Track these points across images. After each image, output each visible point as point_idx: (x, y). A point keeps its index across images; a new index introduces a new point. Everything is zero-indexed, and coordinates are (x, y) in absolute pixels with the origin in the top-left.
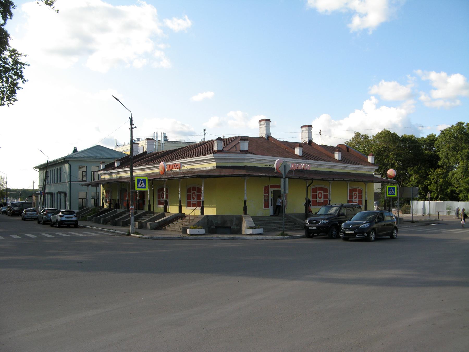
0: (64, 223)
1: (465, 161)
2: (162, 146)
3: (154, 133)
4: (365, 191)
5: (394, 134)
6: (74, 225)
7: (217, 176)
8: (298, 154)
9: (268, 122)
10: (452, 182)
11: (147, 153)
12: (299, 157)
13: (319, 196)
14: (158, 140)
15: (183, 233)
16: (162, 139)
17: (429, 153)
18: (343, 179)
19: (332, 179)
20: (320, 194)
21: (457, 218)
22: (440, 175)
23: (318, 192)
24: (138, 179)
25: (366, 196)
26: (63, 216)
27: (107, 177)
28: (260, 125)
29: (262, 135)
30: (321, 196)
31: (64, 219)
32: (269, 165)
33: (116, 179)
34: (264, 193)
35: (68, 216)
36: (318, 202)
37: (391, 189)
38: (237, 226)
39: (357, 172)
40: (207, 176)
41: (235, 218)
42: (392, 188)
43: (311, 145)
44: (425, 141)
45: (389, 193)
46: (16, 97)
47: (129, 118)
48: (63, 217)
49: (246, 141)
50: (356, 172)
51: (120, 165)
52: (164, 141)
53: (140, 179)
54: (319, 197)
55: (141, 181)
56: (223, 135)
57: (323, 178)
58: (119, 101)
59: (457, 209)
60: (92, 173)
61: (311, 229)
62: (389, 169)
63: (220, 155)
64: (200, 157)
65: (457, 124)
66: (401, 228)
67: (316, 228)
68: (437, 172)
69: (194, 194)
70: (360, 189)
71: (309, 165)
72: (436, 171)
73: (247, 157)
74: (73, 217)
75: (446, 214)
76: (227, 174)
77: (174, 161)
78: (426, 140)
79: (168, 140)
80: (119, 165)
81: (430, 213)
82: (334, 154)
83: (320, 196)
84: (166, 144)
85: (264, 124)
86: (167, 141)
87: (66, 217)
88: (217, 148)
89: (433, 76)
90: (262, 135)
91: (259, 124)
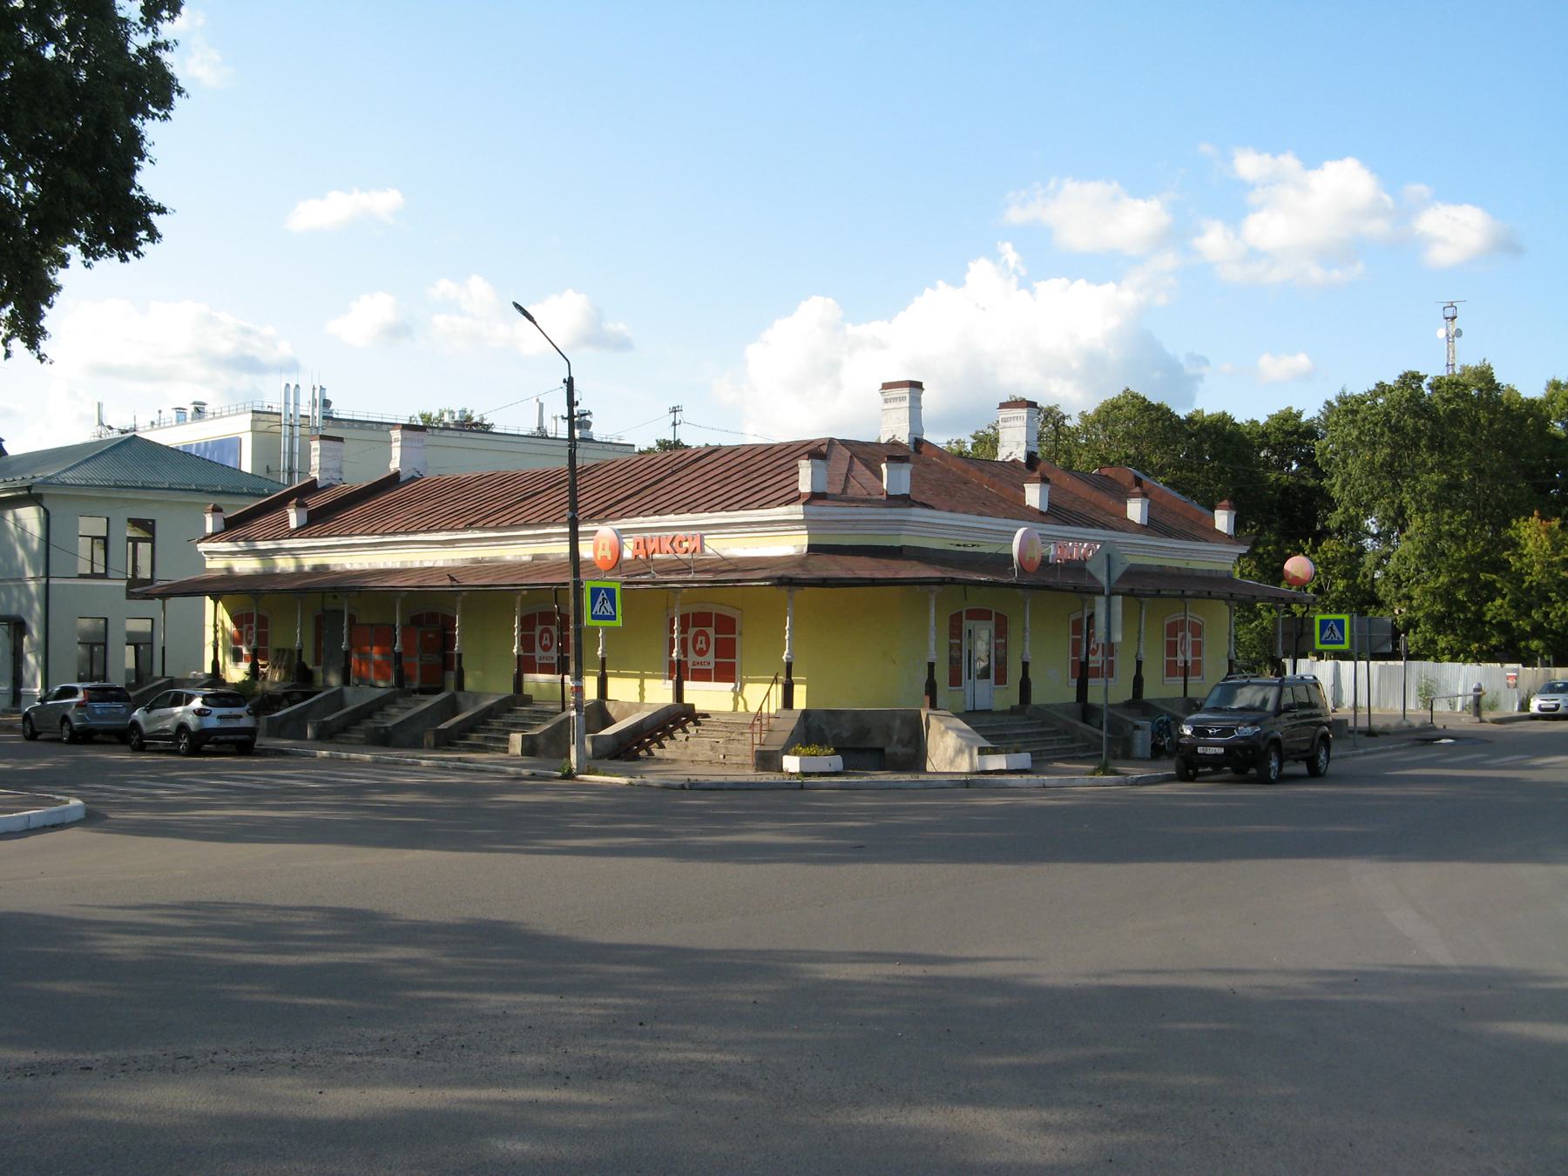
0: (213, 738)
1: (1427, 516)
3: (288, 385)
5: (1159, 408)
6: (243, 745)
10: (1379, 590)
11: (402, 479)
12: (1140, 529)
13: (544, 643)
14: (302, 416)
15: (757, 770)
16: (317, 410)
17: (1280, 482)
18: (1183, 591)
19: (1154, 593)
21: (1477, 719)
22: (1334, 564)
23: (539, 629)
24: (592, 589)
25: (1139, 645)
26: (207, 712)
27: (247, 565)
28: (886, 401)
29: (894, 436)
30: (704, 646)
31: (212, 722)
32: (973, 546)
33: (300, 573)
34: (950, 638)
35: (225, 711)
36: (694, 667)
37: (1330, 625)
38: (904, 746)
39: (1190, 562)
40: (815, 582)
41: (898, 723)
42: (1332, 622)
44: (1264, 435)
45: (1324, 637)
46: (57, 277)
47: (565, 381)
49: (905, 465)
50: (1188, 564)
52: (324, 418)
53: (600, 589)
54: (694, 647)
56: (538, 400)
57: (1132, 590)
58: (535, 323)
59: (1475, 690)
60: (130, 544)
62: (1289, 556)
63: (825, 510)
64: (741, 512)
66: (1365, 754)
67: (1221, 751)
68: (1325, 553)
70: (1196, 621)
71: (1098, 546)
72: (1322, 550)
73: (913, 519)
75: (1417, 705)
76: (878, 575)
77: (611, 522)
78: (1270, 433)
79: (335, 416)
80: (305, 521)
81: (1358, 705)
82: (1126, 503)
85: (903, 399)
86: (332, 418)
87: (220, 717)
88: (810, 483)
89: (1248, 164)
90: (894, 436)
91: (880, 398)
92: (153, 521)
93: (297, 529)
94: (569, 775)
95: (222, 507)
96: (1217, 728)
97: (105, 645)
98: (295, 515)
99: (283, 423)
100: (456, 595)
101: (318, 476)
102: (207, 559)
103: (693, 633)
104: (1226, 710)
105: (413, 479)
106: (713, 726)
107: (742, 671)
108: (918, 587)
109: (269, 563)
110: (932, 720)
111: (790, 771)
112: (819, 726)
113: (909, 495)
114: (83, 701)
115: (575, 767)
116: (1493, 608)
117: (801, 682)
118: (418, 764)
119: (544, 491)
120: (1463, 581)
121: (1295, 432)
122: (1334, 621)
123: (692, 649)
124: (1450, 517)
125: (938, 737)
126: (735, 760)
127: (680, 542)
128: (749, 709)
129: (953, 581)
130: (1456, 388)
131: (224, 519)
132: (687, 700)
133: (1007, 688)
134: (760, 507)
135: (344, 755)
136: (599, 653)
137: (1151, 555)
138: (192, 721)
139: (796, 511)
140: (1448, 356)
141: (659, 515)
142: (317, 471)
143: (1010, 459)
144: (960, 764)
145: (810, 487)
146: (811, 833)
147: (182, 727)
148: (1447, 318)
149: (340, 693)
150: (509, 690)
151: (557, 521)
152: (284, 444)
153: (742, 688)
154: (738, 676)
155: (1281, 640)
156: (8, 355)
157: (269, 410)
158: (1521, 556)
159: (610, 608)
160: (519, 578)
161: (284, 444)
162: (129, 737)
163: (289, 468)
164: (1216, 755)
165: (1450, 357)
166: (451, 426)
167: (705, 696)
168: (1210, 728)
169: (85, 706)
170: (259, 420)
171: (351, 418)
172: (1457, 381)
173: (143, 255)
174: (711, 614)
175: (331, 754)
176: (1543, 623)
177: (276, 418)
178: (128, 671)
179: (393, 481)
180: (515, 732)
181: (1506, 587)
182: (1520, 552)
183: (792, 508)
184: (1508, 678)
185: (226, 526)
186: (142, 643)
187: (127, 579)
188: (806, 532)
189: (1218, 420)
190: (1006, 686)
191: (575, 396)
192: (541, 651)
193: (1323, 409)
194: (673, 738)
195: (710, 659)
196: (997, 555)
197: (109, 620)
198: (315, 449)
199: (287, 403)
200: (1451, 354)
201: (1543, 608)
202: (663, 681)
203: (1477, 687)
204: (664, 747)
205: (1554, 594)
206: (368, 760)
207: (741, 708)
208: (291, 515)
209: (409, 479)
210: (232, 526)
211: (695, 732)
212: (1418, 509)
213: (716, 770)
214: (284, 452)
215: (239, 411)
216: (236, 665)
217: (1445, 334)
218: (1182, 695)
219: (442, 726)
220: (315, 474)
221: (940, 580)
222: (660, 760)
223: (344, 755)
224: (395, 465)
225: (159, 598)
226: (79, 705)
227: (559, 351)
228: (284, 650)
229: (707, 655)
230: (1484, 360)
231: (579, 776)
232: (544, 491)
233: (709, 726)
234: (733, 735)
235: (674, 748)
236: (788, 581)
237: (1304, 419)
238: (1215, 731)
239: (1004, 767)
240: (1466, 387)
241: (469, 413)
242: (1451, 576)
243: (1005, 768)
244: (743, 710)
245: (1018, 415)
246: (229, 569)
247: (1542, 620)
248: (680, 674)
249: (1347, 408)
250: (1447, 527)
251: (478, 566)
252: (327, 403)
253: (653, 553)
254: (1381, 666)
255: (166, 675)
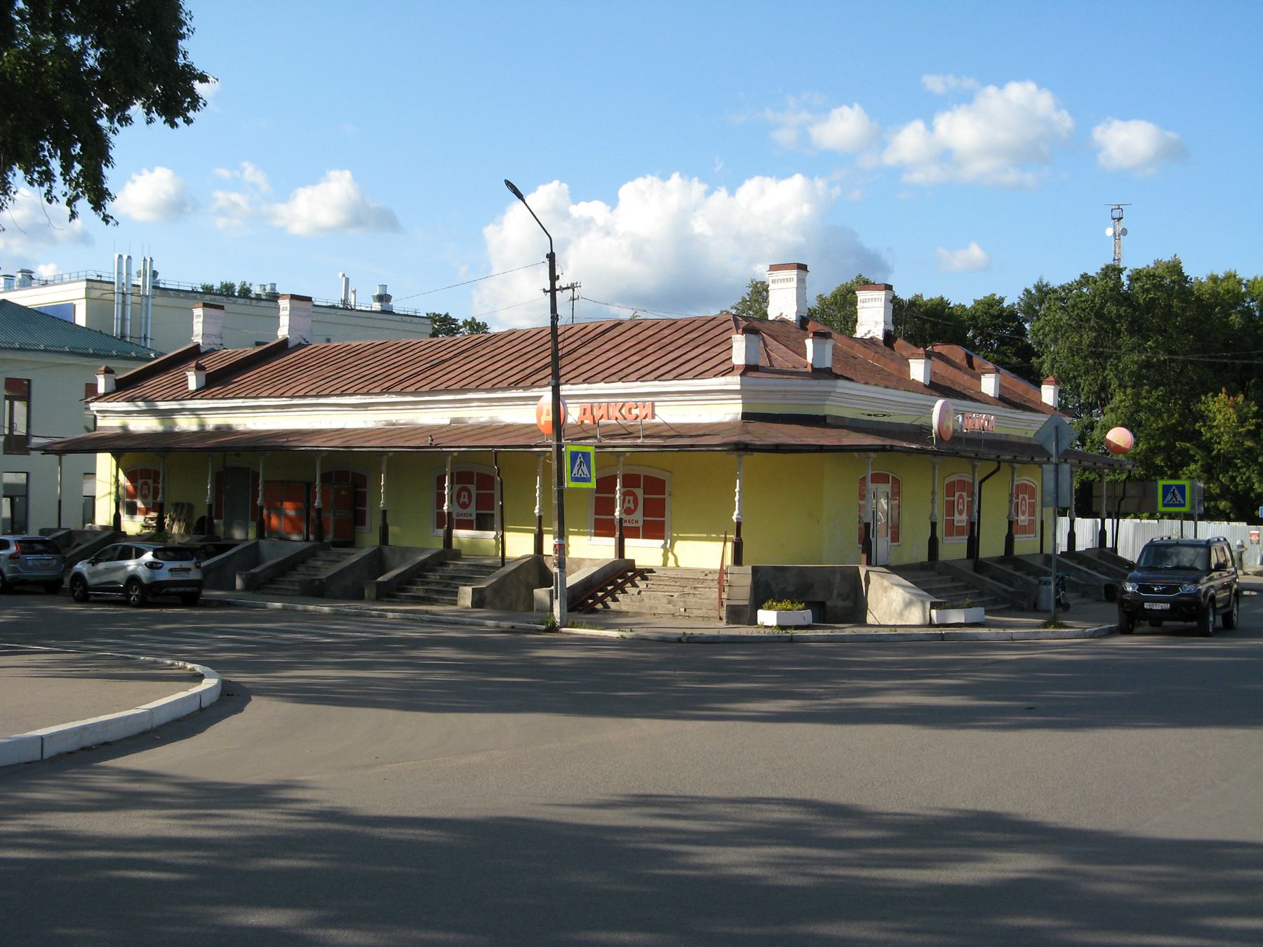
1: (1129, 391)
2: (147, 305)
4: (931, 491)
6: (188, 596)
7: (798, 448)
8: (922, 381)
9: (803, 272)
11: (290, 345)
13: (462, 500)
14: (134, 285)
20: (463, 493)
25: (933, 508)
27: (144, 425)
29: (781, 314)
31: (164, 575)
32: (884, 415)
33: (202, 434)
36: (458, 518)
37: (1172, 490)
41: (838, 578)
42: (1174, 487)
43: (893, 349)
44: (973, 318)
48: (160, 571)
51: (206, 383)
54: (458, 501)
55: (580, 458)
60: (7, 402)
61: (1151, 610)
65: (1103, 269)
67: (1167, 606)
69: (1024, 502)
74: (193, 571)
79: (161, 286)
80: (203, 383)
83: (145, 492)
84: (159, 300)
85: (791, 280)
87: (171, 570)
90: (781, 314)
92: (29, 381)
93: (197, 390)
94: (553, 628)
95: (113, 369)
96: (1162, 586)
97: (26, 496)
98: (194, 377)
99: (116, 291)
100: (382, 455)
101: (200, 341)
102: (98, 417)
103: (457, 489)
104: (1161, 569)
105: (300, 346)
106: (660, 581)
107: (671, 528)
108: (856, 454)
109: (168, 422)
110: (873, 576)
111: (765, 624)
112: (766, 581)
113: (831, 369)
114: (16, 553)
115: (559, 621)
116: (1187, 472)
117: (549, 532)
118: (385, 617)
119: (450, 359)
120: (1160, 448)
121: (1000, 316)
122: (1176, 486)
123: (456, 502)
124: (1148, 392)
125: (880, 592)
126: (696, 612)
127: (630, 409)
128: (680, 564)
129: (892, 449)
130: (1154, 279)
131: (115, 380)
132: (628, 556)
133: (899, 545)
134: (694, 378)
135: (300, 607)
136: (537, 511)
137: (1004, 425)
138: (144, 573)
139: (734, 382)
140: (1115, 252)
141: (588, 383)
142: (201, 337)
143: (868, 336)
144: (908, 617)
145: (744, 360)
146: (291, 656)
147: (133, 579)
148: (1114, 219)
149: (255, 546)
150: (440, 546)
151: (480, 387)
152: (117, 312)
153: (672, 545)
154: (667, 532)
155: (1105, 502)
156: (73, 215)
157: (99, 279)
158: (1211, 428)
159: (586, 472)
160: (454, 440)
161: (117, 312)
162: (83, 592)
163: (121, 333)
164: (1162, 611)
165: (1117, 252)
166: (263, 297)
167: (643, 552)
168: (1155, 586)
169: (18, 558)
170: (93, 288)
171: (176, 288)
172: (1154, 273)
173: (177, 127)
174: (640, 476)
175: (283, 606)
176: (1229, 486)
177: (110, 287)
178: (4, 520)
179: (282, 348)
180: (466, 585)
181: (1198, 453)
182: (1209, 423)
183: (728, 378)
184: (1251, 535)
185: (117, 387)
186: (18, 496)
187: (5, 435)
188: (741, 401)
189: (938, 305)
190: (899, 543)
191: (556, 271)
192: (458, 507)
193: (1022, 296)
194: (624, 592)
195: (638, 518)
196: (921, 427)
197: (31, 475)
198: (198, 316)
199: (120, 273)
200: (1117, 249)
201: (1230, 473)
202: (589, 537)
203: (1240, 544)
204: (619, 601)
205: (1239, 461)
206: (328, 612)
207: (671, 563)
208: (189, 378)
209: (296, 346)
210: (122, 387)
211: (645, 586)
212: (1120, 385)
213: (675, 623)
214: (117, 319)
215: (80, 278)
216: (132, 518)
217: (1113, 232)
218: (1039, 551)
219: (380, 579)
220: (198, 339)
221: (881, 447)
222: (619, 613)
223: (300, 607)
224: (283, 332)
225: (56, 454)
226: (12, 557)
227: (543, 228)
228: (183, 505)
229: (635, 514)
230: (1175, 255)
231: (563, 629)
232: (450, 359)
233: (657, 580)
234: (686, 589)
235: (628, 601)
236: (743, 446)
237: (1005, 305)
238: (1161, 588)
239: (962, 621)
240: (1163, 278)
241: (248, 285)
242: (1149, 443)
243: (963, 622)
244: (674, 565)
245: (877, 297)
246: (124, 428)
247: (1228, 484)
248: (623, 533)
249: (1041, 295)
250: (1146, 401)
251: (392, 431)
252: (155, 274)
253: (601, 419)
254: (1136, 524)
255: (62, 526)
